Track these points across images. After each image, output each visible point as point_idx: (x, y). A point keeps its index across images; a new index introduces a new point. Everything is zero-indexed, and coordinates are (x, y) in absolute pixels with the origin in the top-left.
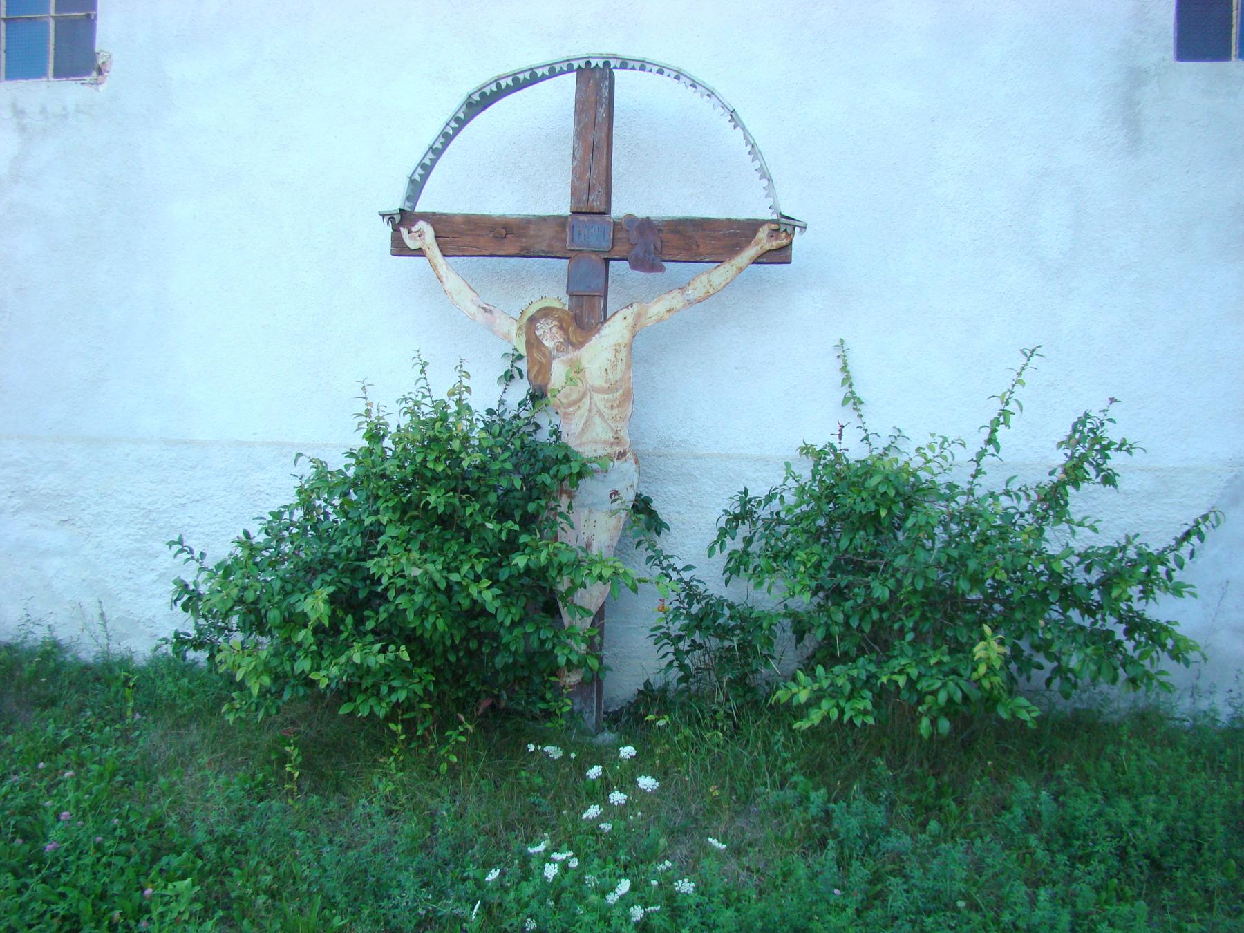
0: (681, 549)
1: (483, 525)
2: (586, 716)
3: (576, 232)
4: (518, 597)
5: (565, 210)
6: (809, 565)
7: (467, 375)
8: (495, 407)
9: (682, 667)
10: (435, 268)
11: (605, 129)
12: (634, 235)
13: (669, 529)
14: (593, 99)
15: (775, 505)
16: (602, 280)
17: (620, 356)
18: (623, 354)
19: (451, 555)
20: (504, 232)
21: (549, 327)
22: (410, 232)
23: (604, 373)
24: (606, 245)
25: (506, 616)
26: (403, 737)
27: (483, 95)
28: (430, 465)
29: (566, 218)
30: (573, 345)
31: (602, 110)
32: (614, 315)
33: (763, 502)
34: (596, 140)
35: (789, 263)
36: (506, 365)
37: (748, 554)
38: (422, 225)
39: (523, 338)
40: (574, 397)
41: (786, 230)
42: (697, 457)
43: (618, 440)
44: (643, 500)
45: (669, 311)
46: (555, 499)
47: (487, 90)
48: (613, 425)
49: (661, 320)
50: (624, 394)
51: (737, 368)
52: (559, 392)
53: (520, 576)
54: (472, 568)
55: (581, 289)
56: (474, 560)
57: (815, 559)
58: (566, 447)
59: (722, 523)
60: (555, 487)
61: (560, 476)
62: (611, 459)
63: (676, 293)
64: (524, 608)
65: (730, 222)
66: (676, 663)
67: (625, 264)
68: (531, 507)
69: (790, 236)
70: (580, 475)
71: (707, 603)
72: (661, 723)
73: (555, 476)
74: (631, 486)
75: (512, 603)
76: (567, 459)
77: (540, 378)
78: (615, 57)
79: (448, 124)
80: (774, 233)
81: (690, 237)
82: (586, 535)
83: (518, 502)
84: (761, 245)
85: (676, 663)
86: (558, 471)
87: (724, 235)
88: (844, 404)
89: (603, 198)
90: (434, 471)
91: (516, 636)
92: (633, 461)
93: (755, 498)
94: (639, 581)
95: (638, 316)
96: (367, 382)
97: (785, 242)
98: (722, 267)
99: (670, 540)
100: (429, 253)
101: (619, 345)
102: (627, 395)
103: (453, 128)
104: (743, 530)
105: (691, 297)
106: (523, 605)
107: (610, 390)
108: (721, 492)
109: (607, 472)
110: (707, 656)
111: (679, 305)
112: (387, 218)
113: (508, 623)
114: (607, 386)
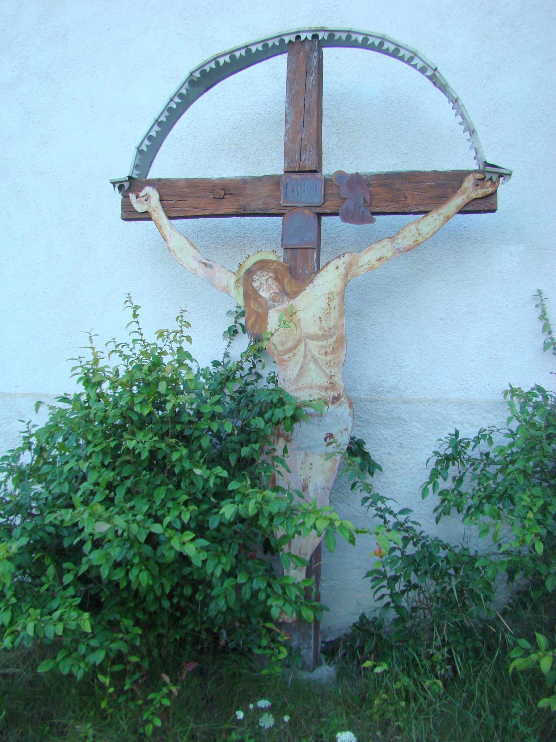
0: (392, 488)
1: (191, 470)
2: (304, 652)
3: (290, 189)
4: (230, 545)
5: (281, 172)
6: (535, 509)
7: (188, 325)
8: (220, 359)
9: (398, 608)
10: (160, 228)
11: (314, 94)
12: (344, 191)
13: (381, 469)
14: (303, 69)
15: (483, 445)
16: (315, 233)
17: (333, 304)
18: (336, 302)
19: (158, 502)
20: (222, 193)
21: (264, 278)
22: (137, 197)
23: (318, 321)
24: (318, 200)
25: (216, 566)
26: (111, 690)
27: (203, 73)
28: (137, 409)
29: (280, 177)
30: (288, 294)
31: (312, 78)
32: (327, 265)
33: (472, 444)
34: (307, 105)
35: (494, 211)
36: (231, 321)
37: (461, 494)
38: (148, 190)
39: (241, 290)
40: (290, 344)
41: (491, 179)
42: (406, 402)
43: (333, 386)
44: (356, 443)
45: (380, 259)
46: (269, 442)
47: (207, 68)
48: (328, 371)
49: (372, 268)
50: (337, 341)
51: (441, 319)
52: (272, 335)
53: (231, 524)
54: (179, 517)
55: (295, 242)
56: (183, 508)
57: (540, 503)
58: (281, 391)
59: (432, 464)
60: (269, 431)
61: (275, 420)
62: (326, 403)
63: (386, 242)
64: (236, 557)
65: (436, 173)
66: (392, 605)
67: (337, 219)
68: (245, 451)
69: (495, 184)
70: (294, 418)
71: (423, 546)
72: (378, 670)
73: (270, 420)
74: (346, 430)
75: (223, 552)
76: (282, 403)
77: (257, 327)
78: (323, 30)
79: (172, 100)
80: (479, 183)
81: (399, 190)
82: (302, 478)
83: (233, 445)
84: (467, 194)
85: (392, 605)
86: (272, 415)
87: (431, 186)
88: (545, 350)
89: (315, 158)
90: (140, 415)
91: (226, 589)
92: (347, 405)
93: (464, 439)
94: (357, 532)
95: (350, 265)
96: (93, 333)
97: (490, 190)
98: (426, 218)
99: (382, 480)
100: (154, 215)
101: (332, 293)
102: (341, 342)
103: (177, 104)
104: (453, 470)
105: (400, 246)
106: (235, 553)
107: (325, 337)
108: (429, 434)
109: (321, 416)
110: (422, 596)
111: (389, 254)
112: (117, 185)
113: (218, 573)
114: (320, 333)
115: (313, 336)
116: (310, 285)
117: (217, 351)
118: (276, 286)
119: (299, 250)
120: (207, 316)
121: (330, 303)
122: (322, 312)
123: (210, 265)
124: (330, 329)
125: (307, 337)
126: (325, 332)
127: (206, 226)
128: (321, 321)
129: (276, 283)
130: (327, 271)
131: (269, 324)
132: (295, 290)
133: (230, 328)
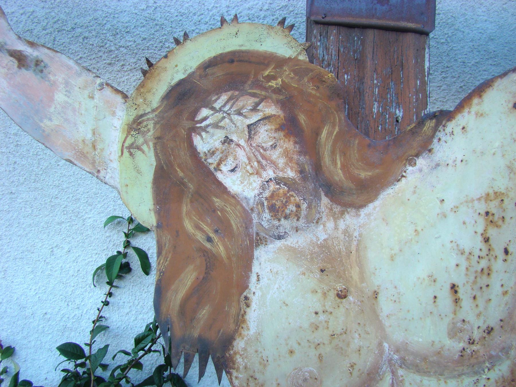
21: (243, 122)
77: (204, 313)
115: (425, 359)
116: (421, 162)
117: (77, 312)
118: (286, 153)
119: (371, 34)
120: (60, 224)
121: (492, 232)
122: (464, 264)
123: (38, 62)
124: (490, 331)
125: (403, 363)
126: (471, 342)
127: (76, 20)
128: (457, 301)
129: (289, 145)
130: (480, 115)
131: (254, 305)
132: (363, 175)
133: (111, 261)
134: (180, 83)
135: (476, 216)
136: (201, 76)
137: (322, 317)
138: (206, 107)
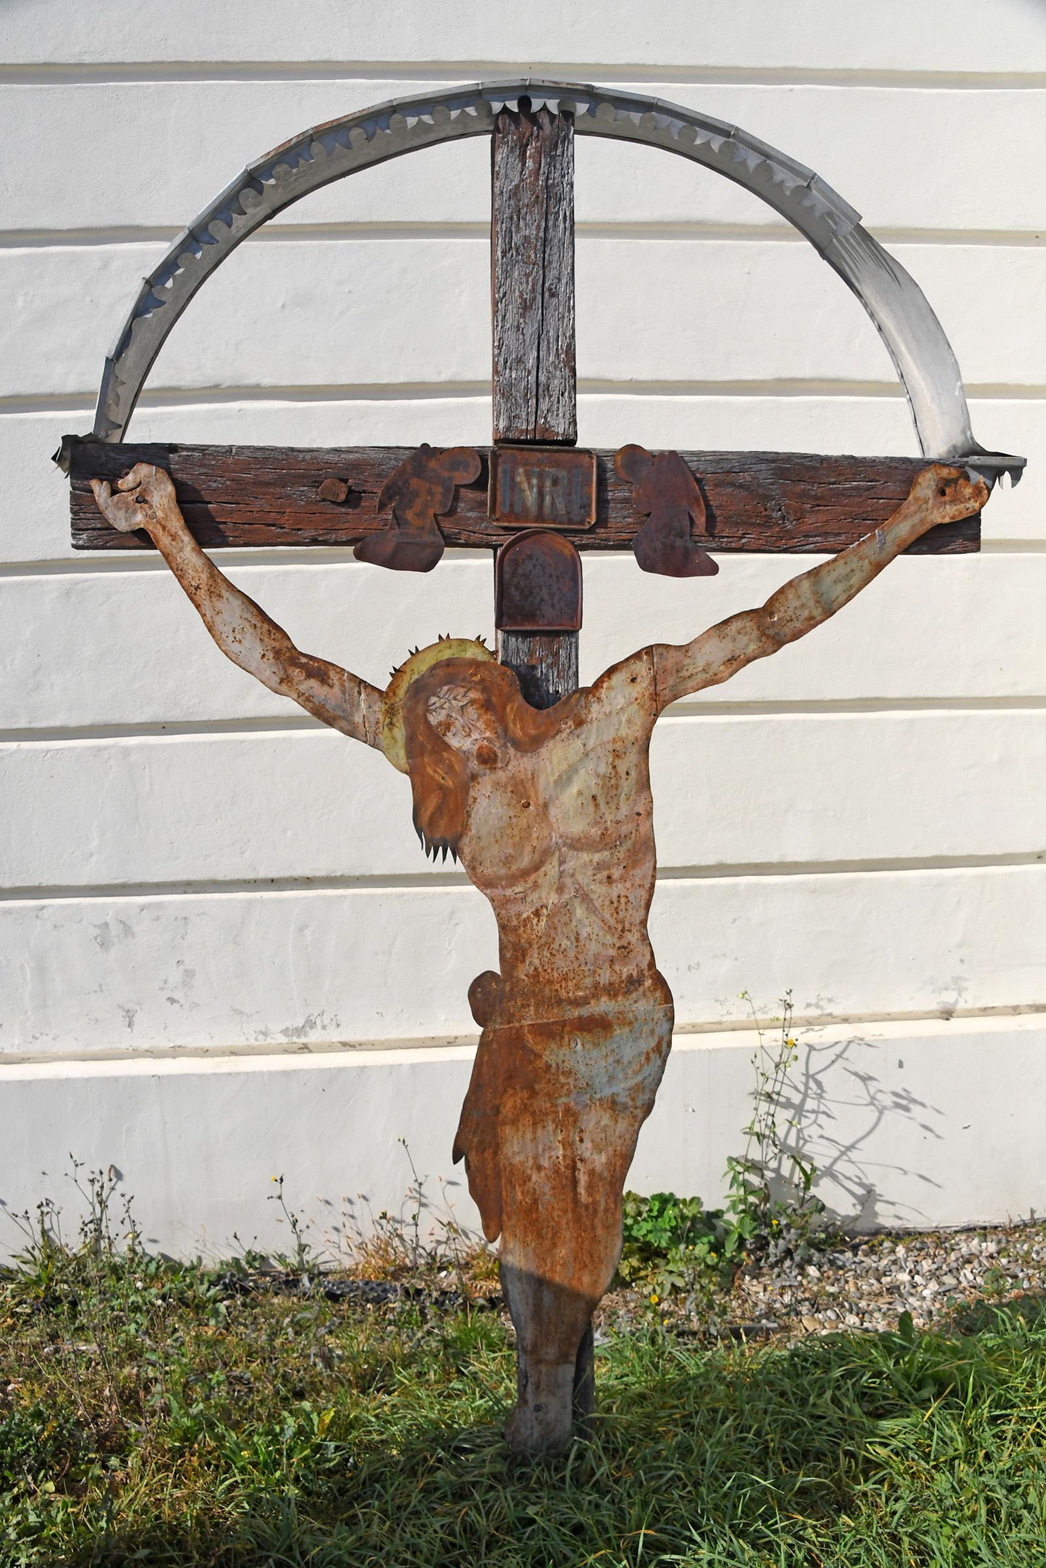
121: (617, 762)
134: (417, 681)
135: (607, 753)
136: (429, 677)
137: (514, 820)
138: (434, 695)
